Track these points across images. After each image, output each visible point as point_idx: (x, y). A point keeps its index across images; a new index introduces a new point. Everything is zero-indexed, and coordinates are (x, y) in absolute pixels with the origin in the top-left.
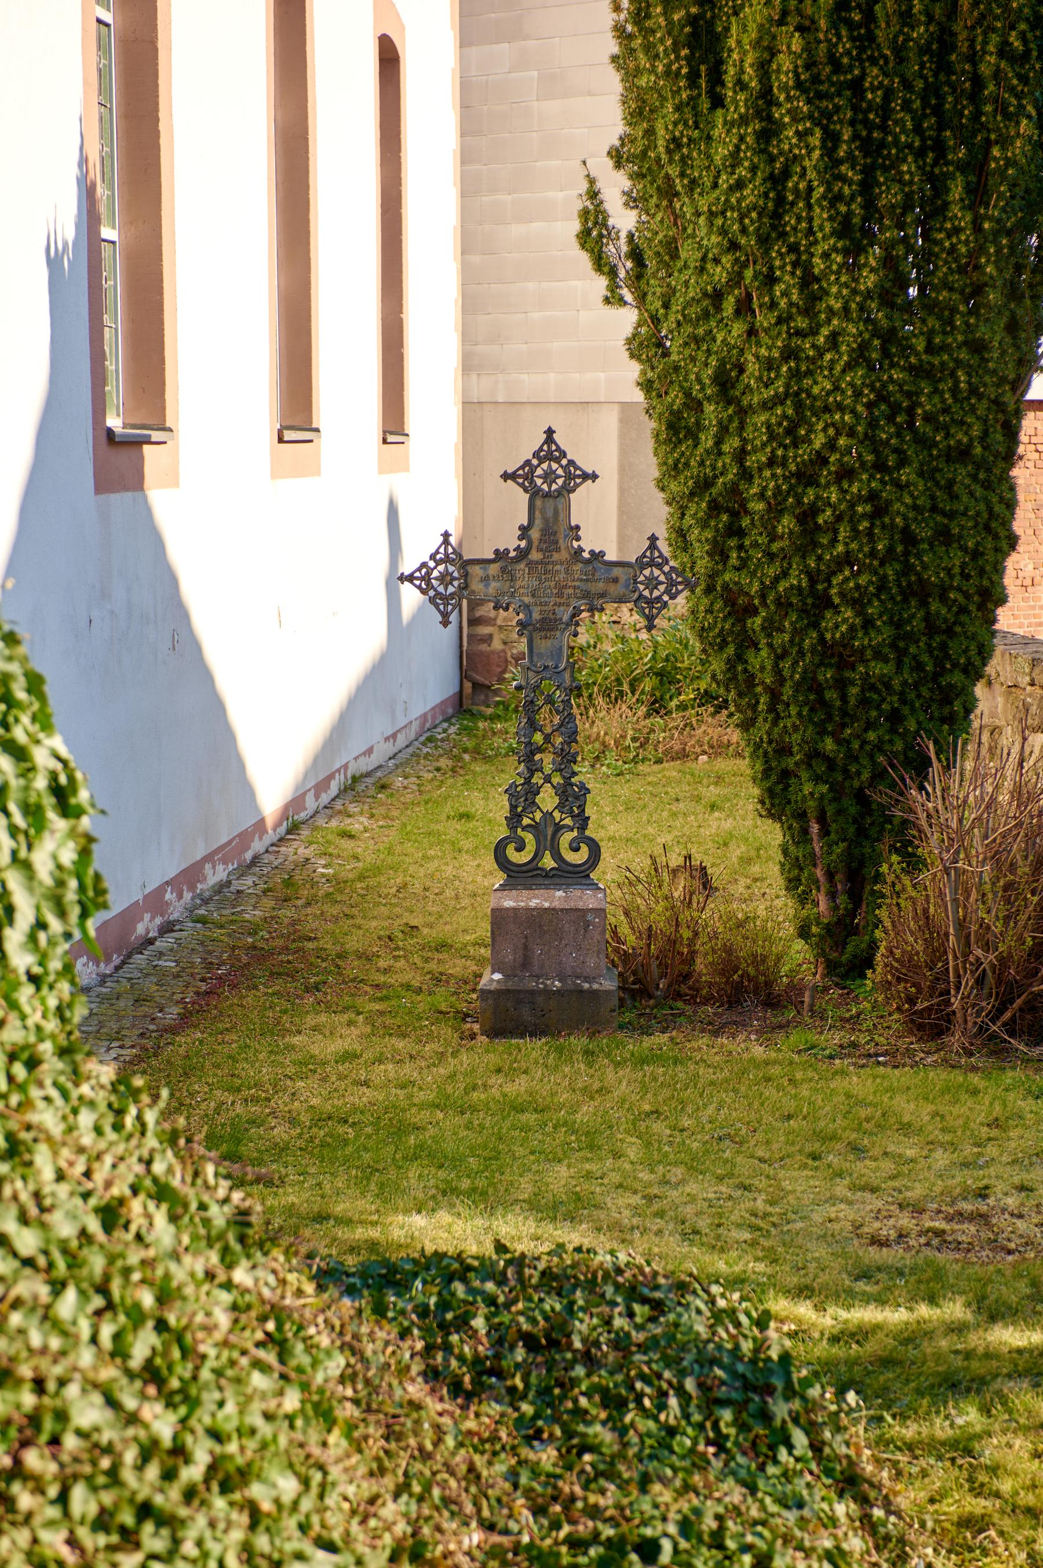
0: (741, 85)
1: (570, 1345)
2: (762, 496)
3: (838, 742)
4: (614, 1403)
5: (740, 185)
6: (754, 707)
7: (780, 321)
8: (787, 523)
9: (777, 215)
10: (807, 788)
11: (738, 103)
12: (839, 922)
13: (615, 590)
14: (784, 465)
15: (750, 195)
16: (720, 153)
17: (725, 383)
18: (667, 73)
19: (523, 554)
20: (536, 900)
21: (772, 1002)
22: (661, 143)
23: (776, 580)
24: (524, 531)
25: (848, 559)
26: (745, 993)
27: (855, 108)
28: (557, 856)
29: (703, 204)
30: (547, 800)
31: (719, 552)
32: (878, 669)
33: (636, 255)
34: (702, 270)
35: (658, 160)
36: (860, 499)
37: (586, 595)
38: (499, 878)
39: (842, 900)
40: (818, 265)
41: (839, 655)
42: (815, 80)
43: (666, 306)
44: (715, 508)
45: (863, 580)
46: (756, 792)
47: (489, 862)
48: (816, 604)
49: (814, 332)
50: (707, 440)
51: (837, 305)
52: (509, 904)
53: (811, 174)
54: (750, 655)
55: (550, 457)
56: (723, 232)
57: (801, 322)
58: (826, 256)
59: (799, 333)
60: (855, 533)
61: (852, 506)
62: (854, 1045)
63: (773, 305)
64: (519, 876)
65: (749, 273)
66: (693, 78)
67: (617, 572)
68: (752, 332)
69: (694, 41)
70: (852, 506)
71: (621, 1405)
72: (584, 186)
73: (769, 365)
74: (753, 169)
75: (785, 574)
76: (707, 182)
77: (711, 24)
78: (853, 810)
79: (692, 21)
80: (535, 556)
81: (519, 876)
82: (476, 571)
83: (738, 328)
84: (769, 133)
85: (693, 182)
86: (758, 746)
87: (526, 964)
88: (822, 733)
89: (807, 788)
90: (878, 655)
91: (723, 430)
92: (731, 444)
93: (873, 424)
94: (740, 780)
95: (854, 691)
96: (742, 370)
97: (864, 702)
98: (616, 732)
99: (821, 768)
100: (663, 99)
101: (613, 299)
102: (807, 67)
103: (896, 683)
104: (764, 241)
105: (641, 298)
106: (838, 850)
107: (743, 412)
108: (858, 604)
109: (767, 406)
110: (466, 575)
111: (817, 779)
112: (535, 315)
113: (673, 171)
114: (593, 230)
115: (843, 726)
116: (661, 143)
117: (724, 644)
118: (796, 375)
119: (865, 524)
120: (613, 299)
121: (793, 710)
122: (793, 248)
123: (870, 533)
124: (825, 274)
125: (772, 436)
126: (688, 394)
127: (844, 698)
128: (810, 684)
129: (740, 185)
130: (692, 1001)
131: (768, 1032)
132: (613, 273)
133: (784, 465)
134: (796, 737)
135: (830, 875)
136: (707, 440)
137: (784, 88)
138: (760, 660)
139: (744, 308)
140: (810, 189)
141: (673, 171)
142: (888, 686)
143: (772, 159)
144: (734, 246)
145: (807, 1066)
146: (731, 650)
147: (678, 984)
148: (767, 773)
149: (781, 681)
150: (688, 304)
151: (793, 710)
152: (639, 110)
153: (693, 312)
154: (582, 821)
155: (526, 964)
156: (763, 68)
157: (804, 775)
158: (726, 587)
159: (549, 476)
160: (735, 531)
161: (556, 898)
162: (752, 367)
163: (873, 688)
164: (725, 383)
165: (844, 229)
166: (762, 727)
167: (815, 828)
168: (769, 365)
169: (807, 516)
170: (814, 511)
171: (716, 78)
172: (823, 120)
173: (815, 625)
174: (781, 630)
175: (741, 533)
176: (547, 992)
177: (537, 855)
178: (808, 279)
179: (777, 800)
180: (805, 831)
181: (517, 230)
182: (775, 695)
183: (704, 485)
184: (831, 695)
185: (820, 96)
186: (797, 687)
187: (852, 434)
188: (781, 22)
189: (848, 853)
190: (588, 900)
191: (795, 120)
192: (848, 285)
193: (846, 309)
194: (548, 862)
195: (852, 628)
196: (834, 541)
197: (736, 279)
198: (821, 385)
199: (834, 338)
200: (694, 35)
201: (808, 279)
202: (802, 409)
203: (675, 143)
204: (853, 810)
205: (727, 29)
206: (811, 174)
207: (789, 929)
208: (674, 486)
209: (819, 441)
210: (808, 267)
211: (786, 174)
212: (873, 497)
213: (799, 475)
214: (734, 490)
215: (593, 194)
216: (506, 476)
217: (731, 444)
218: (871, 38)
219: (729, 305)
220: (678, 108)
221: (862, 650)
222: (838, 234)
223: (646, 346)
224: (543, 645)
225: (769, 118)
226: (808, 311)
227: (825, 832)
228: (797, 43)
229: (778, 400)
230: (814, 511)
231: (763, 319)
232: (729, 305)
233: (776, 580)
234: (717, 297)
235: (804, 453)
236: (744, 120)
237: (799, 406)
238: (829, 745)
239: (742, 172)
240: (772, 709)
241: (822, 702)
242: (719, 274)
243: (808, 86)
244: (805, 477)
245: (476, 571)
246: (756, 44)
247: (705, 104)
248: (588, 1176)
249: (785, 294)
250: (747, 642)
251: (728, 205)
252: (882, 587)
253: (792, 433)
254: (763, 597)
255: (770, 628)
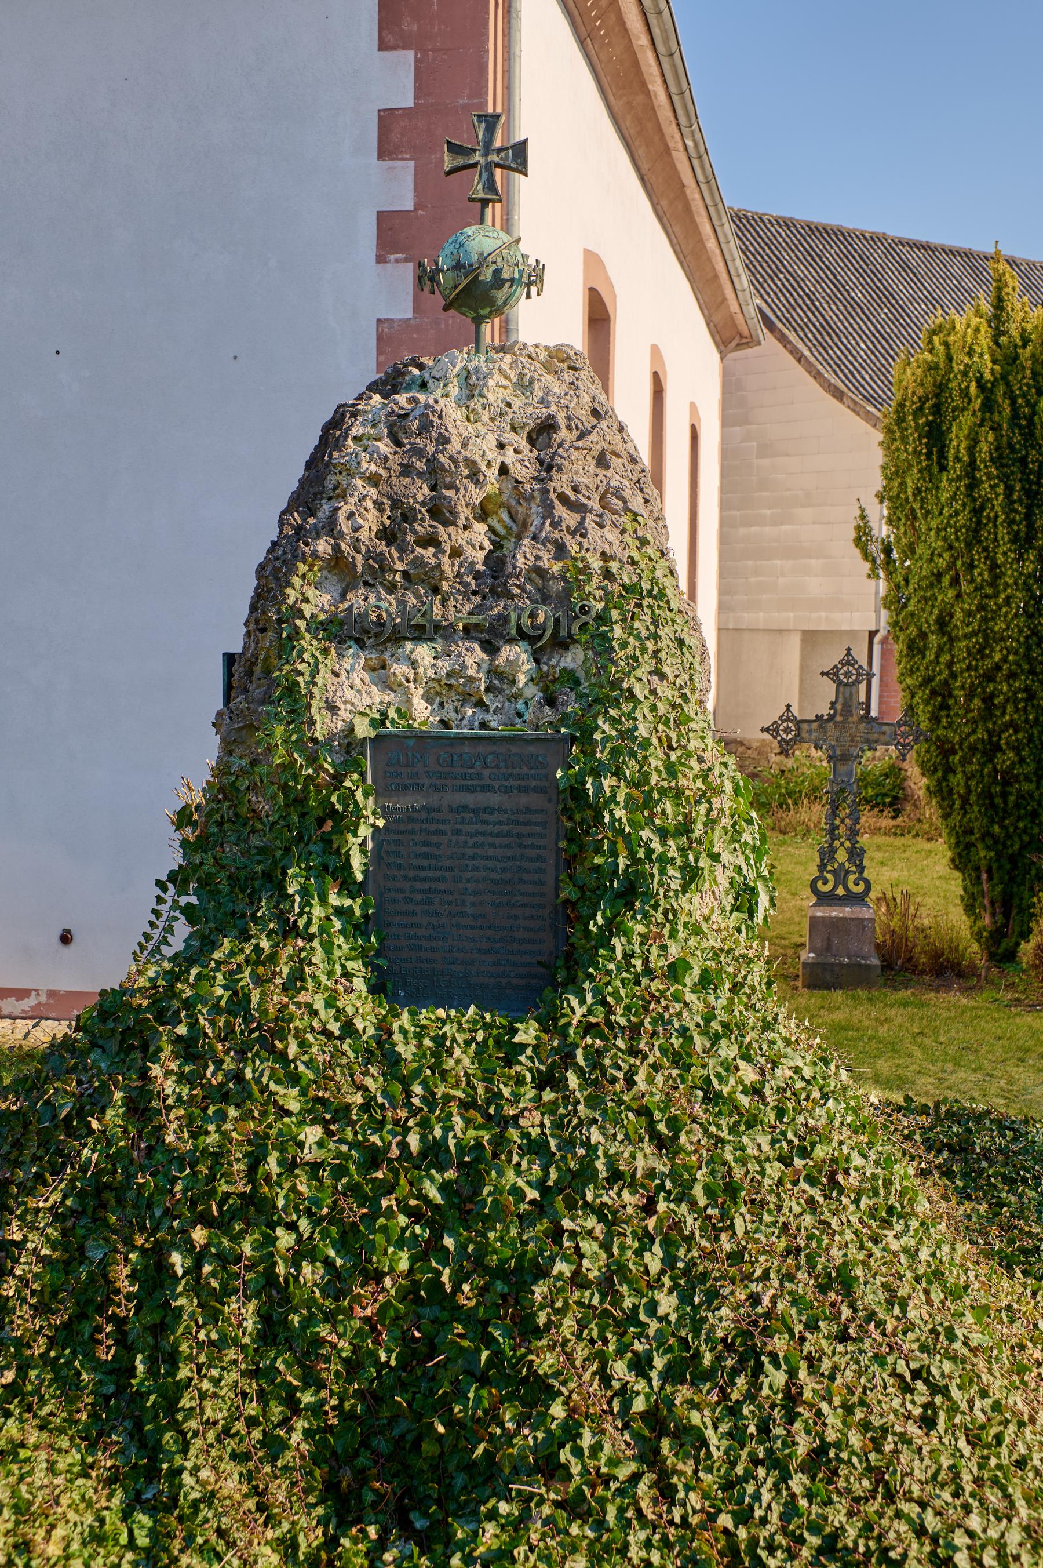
0: (958, 459)
1: (973, 1151)
2: (962, 687)
3: (1002, 827)
4: (1011, 1182)
5: (957, 513)
6: (951, 807)
7: (976, 589)
8: (977, 702)
9: (976, 531)
10: (982, 853)
11: (956, 469)
12: (998, 930)
13: (883, 738)
14: (976, 669)
15: (962, 520)
16: (944, 497)
17: (943, 623)
18: (915, 451)
19: (831, 717)
20: (835, 912)
21: (960, 975)
22: (909, 490)
23: (969, 735)
24: (833, 705)
25: (1012, 724)
26: (944, 969)
27: (1023, 473)
28: (846, 888)
29: (934, 524)
30: (841, 856)
31: (935, 719)
32: (1026, 786)
33: (887, 550)
34: (931, 560)
35: (907, 500)
36: (1020, 690)
37: (867, 741)
38: (814, 900)
39: (1000, 918)
40: (1000, 559)
41: (1008, 779)
42: (1001, 457)
43: (907, 581)
44: (934, 693)
45: (1020, 736)
46: (949, 854)
47: (808, 892)
48: (992, 749)
49: (996, 595)
50: (930, 655)
51: (1011, 581)
52: (819, 914)
53: (997, 508)
54: (951, 777)
55: (848, 663)
56: (945, 539)
57: (989, 591)
58: (1005, 554)
59: (987, 596)
60: (1017, 710)
61: (1015, 694)
62: (1018, 1000)
63: (972, 581)
64: (825, 899)
65: (959, 563)
66: (929, 455)
67: (885, 728)
68: (958, 596)
69: (929, 435)
70: (1015, 694)
71: (1013, 1182)
72: (858, 513)
73: (969, 614)
74: (964, 505)
75: (974, 732)
76: (936, 512)
77: (939, 426)
78: (1008, 867)
79: (929, 423)
80: (838, 718)
81: (825, 899)
82: (805, 726)
83: (951, 593)
84: (973, 485)
85: (928, 512)
86: (953, 829)
87: (828, 948)
88: (992, 822)
89: (982, 853)
90: (1027, 779)
91: (940, 650)
92: (945, 658)
93: (1029, 649)
94: (942, 850)
95: (1012, 798)
96: (952, 616)
97: (1017, 805)
98: (815, 819)
99: (990, 842)
100: (910, 466)
101: (873, 575)
102: (997, 449)
103: (1036, 795)
104: (969, 545)
105: (890, 574)
106: (999, 888)
107: (951, 640)
108: (1017, 750)
109: (966, 637)
110: (798, 729)
111: (988, 848)
112: (752, 580)
113: (916, 506)
114: (862, 537)
115: (1003, 819)
116: (909, 490)
117: (935, 771)
118: (985, 620)
119: (1021, 705)
120: (873, 575)
121: (976, 809)
122: (986, 549)
123: (1025, 709)
124: (1004, 564)
125: (969, 654)
126: (920, 629)
127: (1005, 802)
128: (987, 795)
129: (957, 513)
130: (913, 972)
131: (967, 990)
132: (874, 561)
133: (976, 669)
134: (977, 824)
135: (992, 903)
136: (930, 655)
137: (983, 461)
138: (957, 780)
139: (955, 581)
140: (996, 517)
141: (916, 506)
142: (1031, 796)
143: (974, 500)
144: (951, 547)
145: (998, 1010)
146: (940, 774)
147: (907, 964)
148: (958, 844)
149: (969, 792)
150: (921, 579)
151: (976, 809)
152: (894, 473)
153: (924, 584)
154: (861, 869)
155: (828, 948)
156: (971, 450)
157: (980, 846)
158: (938, 738)
159: (847, 674)
160: (944, 706)
161: (846, 912)
162: (959, 614)
163: (1023, 797)
164: (943, 623)
165: (1015, 539)
166: (956, 818)
167: (985, 876)
168: (969, 614)
169: (988, 699)
170: (992, 696)
171: (942, 455)
172: (1005, 478)
173: (991, 761)
174: (970, 763)
175: (948, 708)
176: (841, 965)
177: (835, 888)
178: (994, 566)
179: (962, 861)
180: (979, 878)
181: (742, 531)
182: (965, 801)
183: (927, 680)
184: (998, 801)
185: (1003, 466)
186: (979, 796)
187: (1016, 653)
188: (981, 425)
189: (1004, 891)
190: (865, 913)
191: (989, 478)
192: (1019, 570)
193: (1016, 583)
194: (840, 891)
195: (1013, 763)
196: (1004, 713)
197: (951, 565)
198: (999, 626)
199: (1008, 601)
200: (930, 432)
201: (994, 566)
202: (987, 640)
203: (918, 491)
204: (1008, 867)
205: (950, 428)
206: (997, 508)
207: (966, 933)
208: (909, 681)
209: (997, 657)
210: (994, 560)
211: (982, 508)
212: (1027, 690)
213: (984, 675)
214: (946, 683)
215: (863, 517)
216: (823, 674)
217: (945, 658)
218: (1032, 435)
219: (946, 580)
220: (920, 471)
221: (1017, 776)
222: (1013, 542)
223: (895, 602)
224: (842, 769)
225: (974, 477)
226: (992, 584)
227: (990, 878)
228: (991, 437)
229: (974, 634)
230: (992, 696)
231: (965, 587)
232: (946, 580)
233: (969, 735)
234: (939, 576)
235: (988, 663)
236: (959, 478)
237: (986, 637)
238: (996, 829)
239: (957, 506)
240: (962, 807)
241: (992, 805)
242: (942, 563)
243: (997, 460)
244: (989, 677)
245: (805, 726)
246: (967, 437)
247: (935, 469)
248: (898, 1066)
249: (980, 574)
250: (949, 770)
251: (948, 524)
252: (1030, 740)
253: (981, 652)
254: (961, 744)
255: (964, 761)
